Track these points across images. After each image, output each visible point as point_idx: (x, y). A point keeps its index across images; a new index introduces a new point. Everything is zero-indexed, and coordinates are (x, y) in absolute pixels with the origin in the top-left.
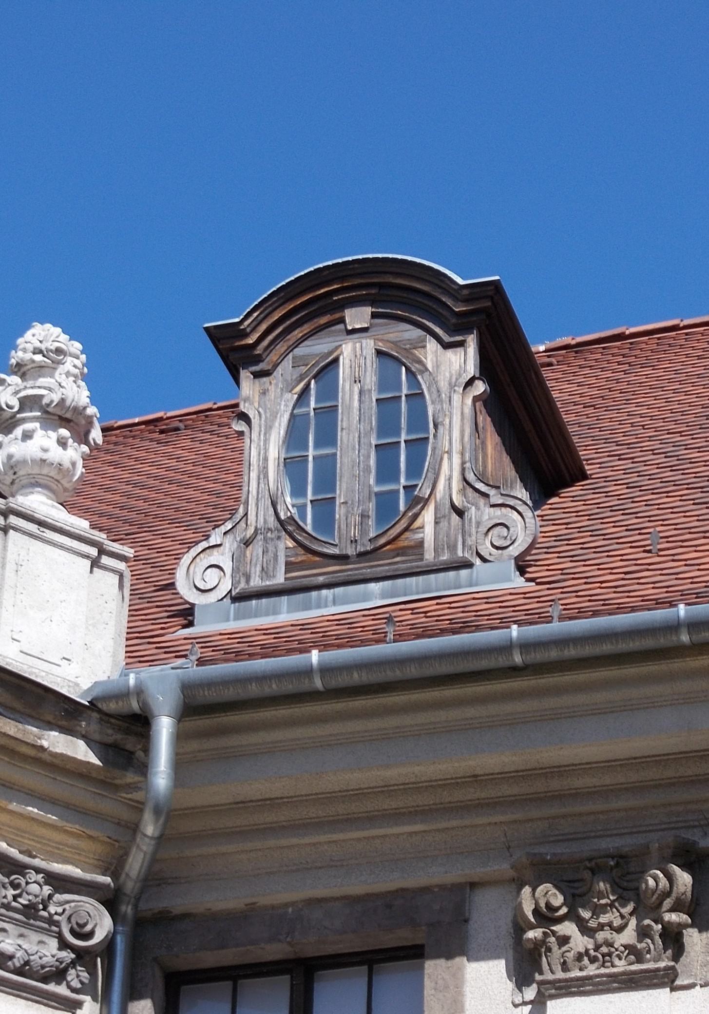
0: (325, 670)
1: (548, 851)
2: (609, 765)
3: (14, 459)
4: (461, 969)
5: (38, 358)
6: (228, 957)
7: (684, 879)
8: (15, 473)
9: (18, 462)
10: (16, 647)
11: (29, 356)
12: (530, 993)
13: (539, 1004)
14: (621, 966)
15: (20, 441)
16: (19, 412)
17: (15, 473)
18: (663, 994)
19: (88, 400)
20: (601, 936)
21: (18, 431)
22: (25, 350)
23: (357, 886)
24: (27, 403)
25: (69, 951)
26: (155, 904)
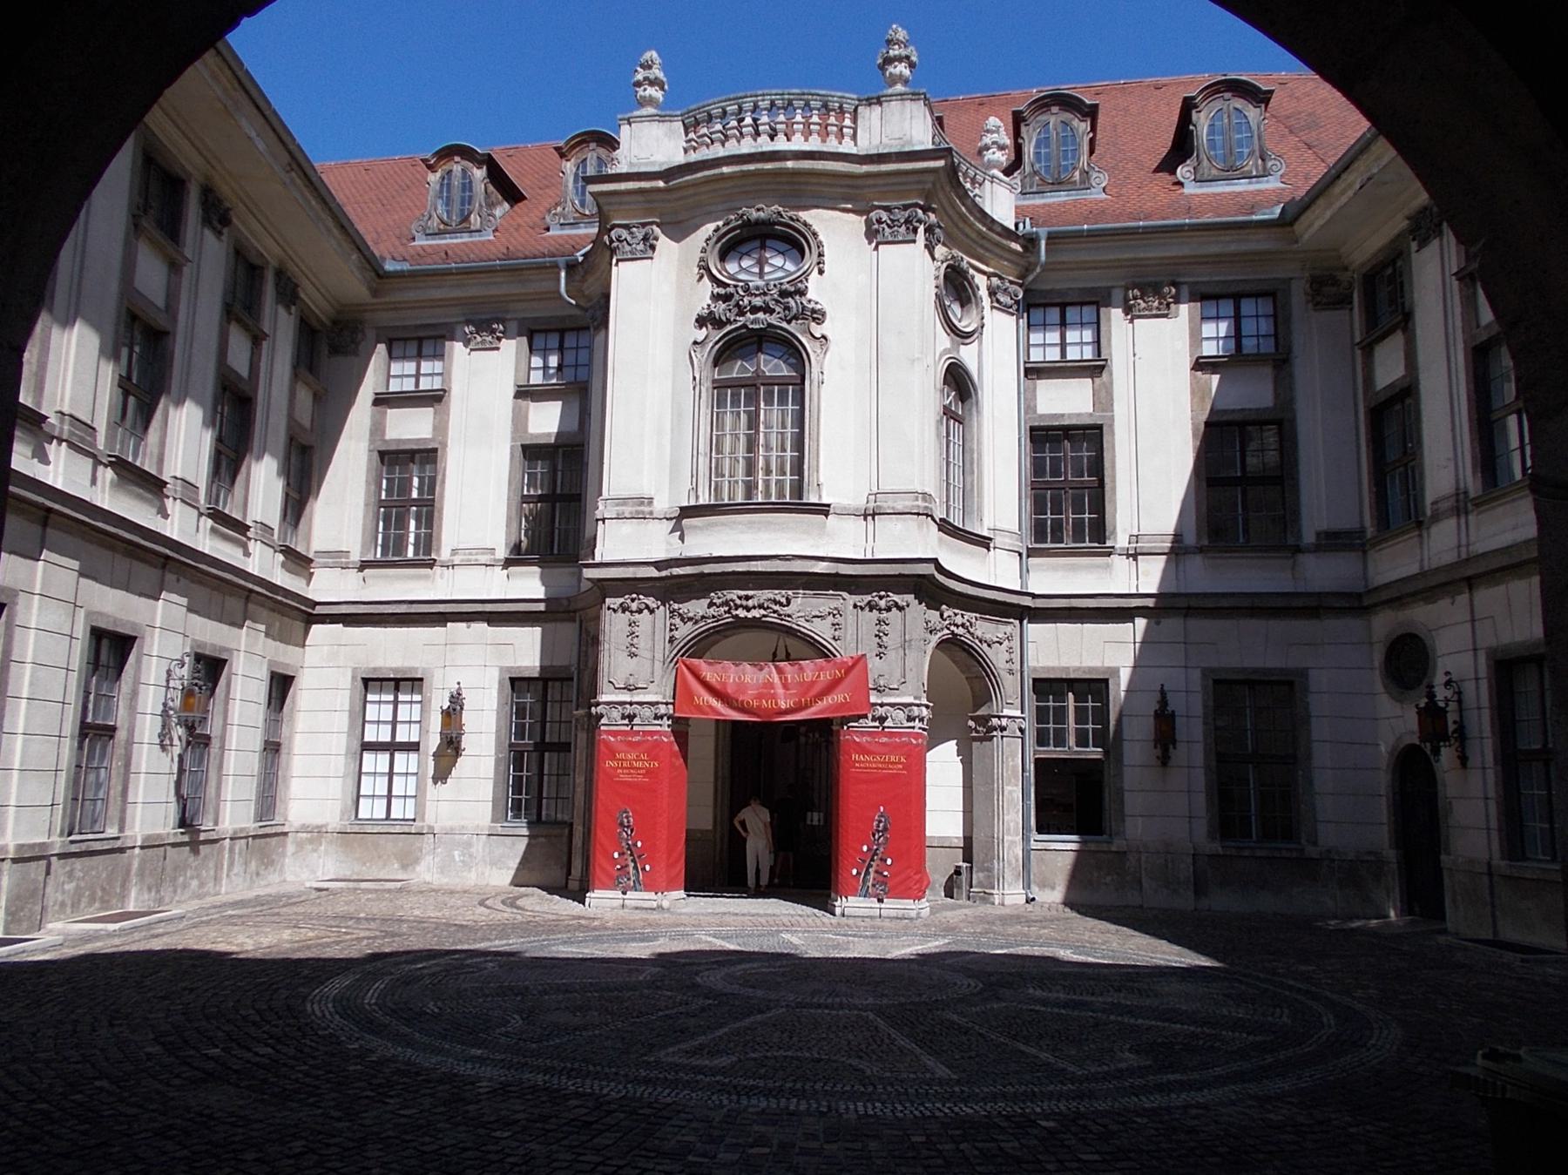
0: (1088, 230)
1: (1137, 280)
2: (1155, 259)
4: (1109, 313)
6: (1043, 301)
7: (1174, 290)
12: (874, 245)
13: (876, 248)
14: (1154, 312)
18: (1164, 320)
23: (1081, 285)
24: (994, 143)
25: (457, 159)
26: (1034, 287)
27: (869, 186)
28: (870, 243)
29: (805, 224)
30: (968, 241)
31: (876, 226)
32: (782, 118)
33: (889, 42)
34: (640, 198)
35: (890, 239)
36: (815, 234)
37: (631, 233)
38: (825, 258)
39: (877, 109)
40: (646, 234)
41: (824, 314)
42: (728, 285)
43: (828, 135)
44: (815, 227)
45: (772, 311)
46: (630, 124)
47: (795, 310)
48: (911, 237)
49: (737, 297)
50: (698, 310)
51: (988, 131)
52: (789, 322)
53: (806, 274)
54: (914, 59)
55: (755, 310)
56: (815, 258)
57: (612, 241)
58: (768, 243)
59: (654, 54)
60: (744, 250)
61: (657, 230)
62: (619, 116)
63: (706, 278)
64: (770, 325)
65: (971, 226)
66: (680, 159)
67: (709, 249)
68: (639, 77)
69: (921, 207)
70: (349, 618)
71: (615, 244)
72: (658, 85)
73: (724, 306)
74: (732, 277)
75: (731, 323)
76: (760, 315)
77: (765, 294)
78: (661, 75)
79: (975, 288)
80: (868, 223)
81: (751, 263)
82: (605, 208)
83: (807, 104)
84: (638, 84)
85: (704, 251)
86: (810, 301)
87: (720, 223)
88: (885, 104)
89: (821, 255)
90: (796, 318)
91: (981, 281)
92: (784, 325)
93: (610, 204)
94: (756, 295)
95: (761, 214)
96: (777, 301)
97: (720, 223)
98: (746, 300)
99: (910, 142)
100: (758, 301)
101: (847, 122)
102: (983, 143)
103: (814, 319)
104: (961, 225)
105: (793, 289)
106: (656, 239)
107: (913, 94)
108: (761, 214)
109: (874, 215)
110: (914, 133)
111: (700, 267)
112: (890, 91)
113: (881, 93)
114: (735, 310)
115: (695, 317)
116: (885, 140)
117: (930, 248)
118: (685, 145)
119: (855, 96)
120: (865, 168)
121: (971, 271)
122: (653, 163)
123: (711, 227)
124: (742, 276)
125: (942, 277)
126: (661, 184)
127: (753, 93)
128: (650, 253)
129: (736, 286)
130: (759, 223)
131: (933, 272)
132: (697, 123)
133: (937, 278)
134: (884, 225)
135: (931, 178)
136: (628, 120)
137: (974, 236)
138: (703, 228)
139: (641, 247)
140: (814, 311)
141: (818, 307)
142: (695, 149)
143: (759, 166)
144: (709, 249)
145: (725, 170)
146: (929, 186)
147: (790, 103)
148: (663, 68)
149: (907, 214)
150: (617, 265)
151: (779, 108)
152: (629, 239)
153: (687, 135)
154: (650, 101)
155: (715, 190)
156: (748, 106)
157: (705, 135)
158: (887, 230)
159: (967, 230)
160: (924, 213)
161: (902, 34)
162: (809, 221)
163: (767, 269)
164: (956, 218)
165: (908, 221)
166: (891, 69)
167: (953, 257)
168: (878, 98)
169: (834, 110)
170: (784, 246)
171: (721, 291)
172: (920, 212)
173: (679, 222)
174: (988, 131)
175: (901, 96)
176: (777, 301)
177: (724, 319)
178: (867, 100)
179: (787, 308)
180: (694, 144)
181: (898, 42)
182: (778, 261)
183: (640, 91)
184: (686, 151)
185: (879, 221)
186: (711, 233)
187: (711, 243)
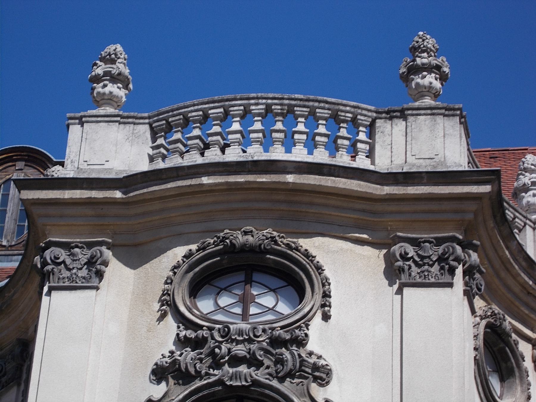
3: (530, 203)
5: (533, 167)
8: (529, 207)
9: (531, 204)
10: (86, 163)
11: (530, 166)
12: (396, 287)
13: (400, 292)
15: (532, 197)
16: (530, 186)
17: (529, 207)
19: (128, 74)
20: (423, 268)
21: (101, 84)
22: (528, 164)
27: (391, 213)
28: (391, 285)
29: (307, 254)
30: (509, 296)
31: (400, 263)
32: (279, 126)
33: (415, 50)
34: (88, 211)
35: (419, 280)
36: (319, 269)
37: (73, 255)
38: (332, 300)
39: (400, 125)
40: (92, 257)
41: (329, 373)
42: (201, 327)
43: (337, 149)
44: (320, 259)
45: (258, 364)
46: (82, 124)
47: (290, 365)
48: (446, 279)
49: (211, 343)
50: (157, 358)
51: (526, 170)
52: (282, 380)
53: (306, 319)
54: (446, 70)
55: (235, 361)
56: (318, 299)
57: (45, 263)
58: (256, 276)
59: (119, 48)
60: (223, 284)
61: (108, 254)
62: (68, 115)
63: (169, 319)
64: (256, 383)
65: (515, 277)
66: (144, 166)
67: (176, 279)
68: (99, 71)
69: (460, 243)
70: (303, 133)
71: (49, 268)
72: (121, 82)
73: (192, 354)
74: (204, 318)
75: (201, 378)
76: (243, 369)
77: (250, 341)
78: (126, 71)
79: (519, 358)
80: (389, 259)
81: (231, 301)
82: (40, 222)
83: (312, 113)
84: (97, 79)
85: (169, 281)
86: (311, 354)
87: (194, 247)
88: (411, 119)
89: (326, 295)
90: (291, 375)
91: (525, 348)
92: (275, 383)
93: (47, 216)
94: (238, 342)
95: (250, 238)
96: (267, 352)
97: (194, 247)
98: (224, 348)
99: (443, 163)
100: (240, 350)
101: (362, 136)
102: (521, 183)
103: (316, 379)
104: (503, 274)
105: (288, 337)
106: (106, 263)
107: (446, 109)
108: (250, 238)
109: (397, 249)
110: (448, 154)
111: (162, 303)
112: (417, 104)
113: (405, 106)
114: (209, 361)
115: (150, 367)
116: (410, 159)
117: (469, 295)
118: (151, 152)
119: (372, 108)
120: (387, 190)
121: (514, 336)
122: (109, 170)
123: (180, 252)
124: (219, 317)
125: (481, 337)
126: (118, 194)
127: (246, 95)
128: (95, 282)
129: (210, 329)
130: (246, 249)
131: (472, 332)
132: (169, 129)
133: (476, 336)
134: (410, 263)
135: (473, 206)
136: (80, 118)
137: (517, 289)
138: (170, 253)
139: (84, 273)
140: (316, 367)
141: (322, 362)
142: (164, 157)
143: (251, 178)
144: (176, 279)
145: (205, 180)
146: (470, 216)
147: (291, 110)
148: (129, 64)
149: (441, 250)
150: (49, 294)
151: (277, 114)
152: (68, 261)
153: (154, 140)
154: (111, 99)
155: (189, 206)
156: (237, 110)
157: (178, 141)
158: (415, 270)
159: (510, 281)
160: (463, 251)
161: (430, 42)
162: (313, 251)
163: (253, 310)
164: (497, 264)
165: (442, 259)
166: (418, 80)
167: (493, 314)
168: (402, 111)
169: (344, 121)
170: (276, 282)
171: (191, 334)
172: (459, 249)
173: (136, 245)
174: (526, 170)
175: (432, 111)
176: (267, 352)
177: (192, 370)
178: (388, 112)
179: (280, 361)
180: (162, 150)
181: (426, 50)
182: (268, 300)
183: (99, 88)
184: (152, 159)
185: (404, 257)
186: (180, 259)
187: (180, 272)
